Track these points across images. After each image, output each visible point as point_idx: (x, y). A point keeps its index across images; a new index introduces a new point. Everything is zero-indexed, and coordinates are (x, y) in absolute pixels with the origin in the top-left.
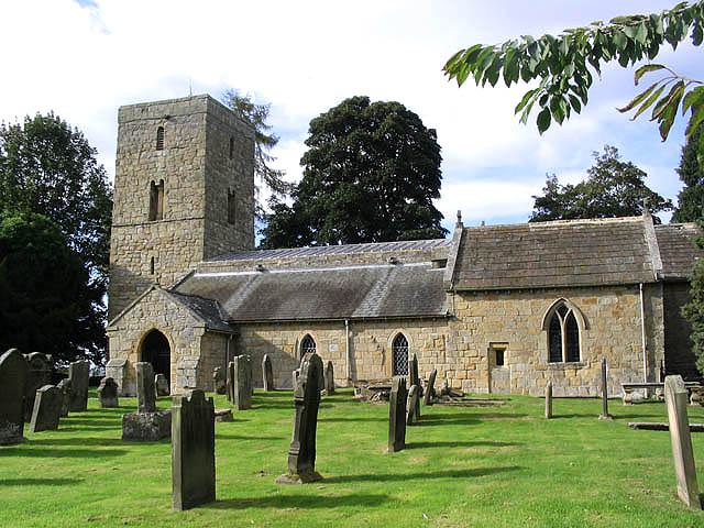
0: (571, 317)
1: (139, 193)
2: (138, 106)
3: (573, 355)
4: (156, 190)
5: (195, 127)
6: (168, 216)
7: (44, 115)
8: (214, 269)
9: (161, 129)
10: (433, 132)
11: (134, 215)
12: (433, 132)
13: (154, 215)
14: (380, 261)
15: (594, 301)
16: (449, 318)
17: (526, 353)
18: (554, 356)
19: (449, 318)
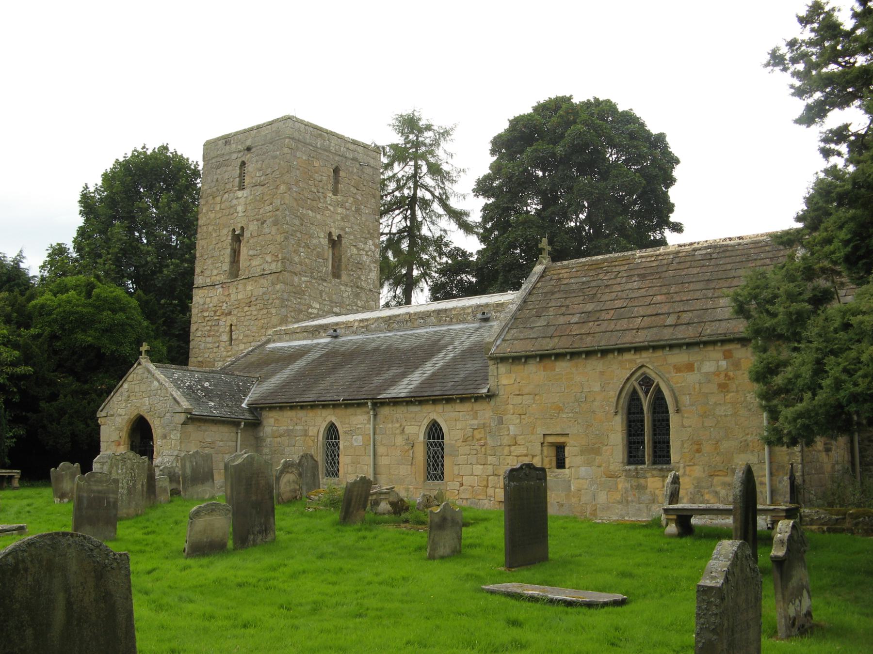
0: (659, 391)
1: (219, 245)
2: (219, 139)
3: (662, 455)
4: (237, 238)
5: (274, 157)
6: (247, 272)
7: (121, 159)
8: (287, 338)
9: (243, 164)
10: (661, 137)
11: (215, 272)
12: (661, 137)
13: (235, 271)
14: (470, 318)
15: (690, 367)
16: (490, 396)
17: (591, 451)
18: (633, 455)
19: (490, 396)
